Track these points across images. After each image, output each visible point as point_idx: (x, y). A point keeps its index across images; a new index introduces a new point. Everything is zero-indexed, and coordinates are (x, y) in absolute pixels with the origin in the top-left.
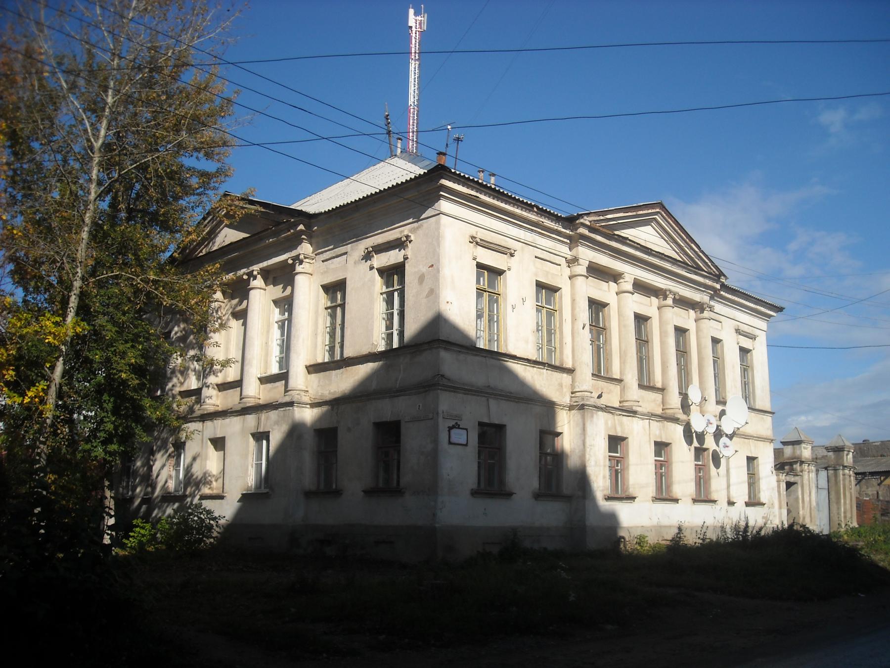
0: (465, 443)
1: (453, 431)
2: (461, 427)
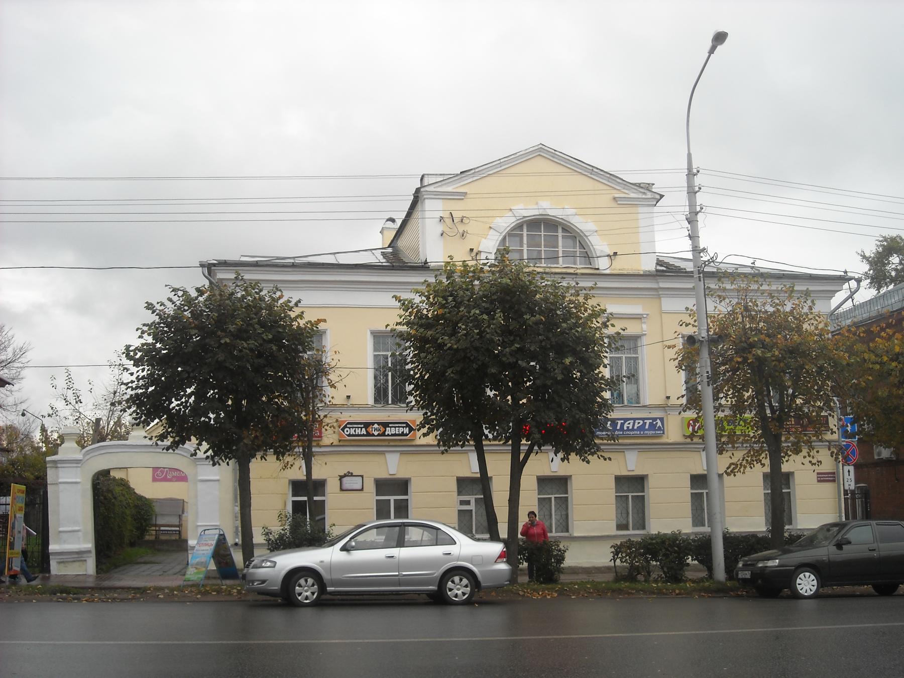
0: (359, 486)
1: (345, 480)
2: (354, 474)
